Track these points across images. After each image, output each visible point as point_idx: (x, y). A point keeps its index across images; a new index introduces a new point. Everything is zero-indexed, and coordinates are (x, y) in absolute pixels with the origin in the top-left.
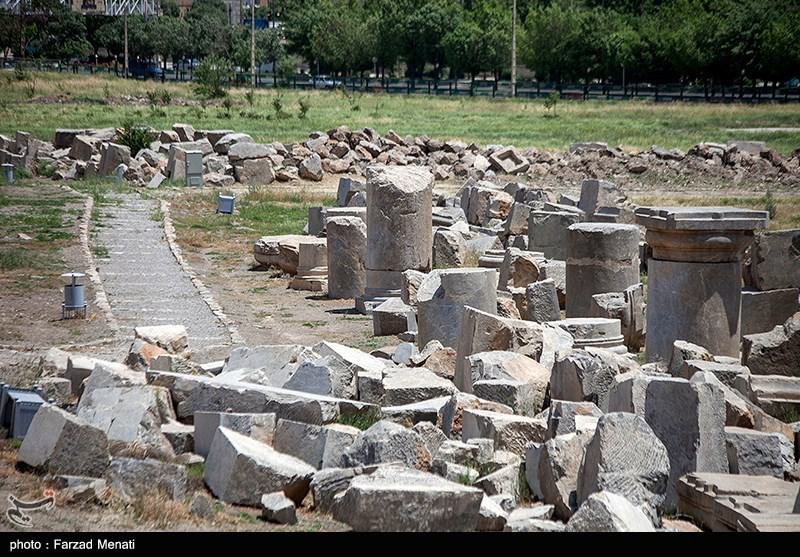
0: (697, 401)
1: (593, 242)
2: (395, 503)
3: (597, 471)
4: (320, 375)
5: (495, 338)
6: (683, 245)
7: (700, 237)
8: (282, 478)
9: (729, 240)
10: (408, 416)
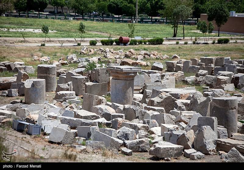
0: (214, 121)
1: (47, 70)
2: (167, 150)
3: (203, 140)
4: (71, 113)
5: (98, 102)
6: (124, 76)
7: (128, 74)
8: (120, 144)
9: (134, 75)
10: (105, 124)
